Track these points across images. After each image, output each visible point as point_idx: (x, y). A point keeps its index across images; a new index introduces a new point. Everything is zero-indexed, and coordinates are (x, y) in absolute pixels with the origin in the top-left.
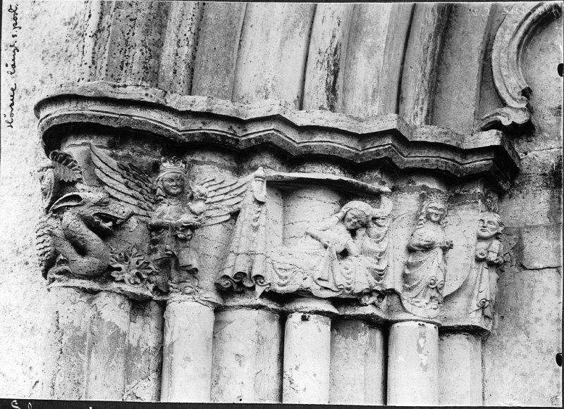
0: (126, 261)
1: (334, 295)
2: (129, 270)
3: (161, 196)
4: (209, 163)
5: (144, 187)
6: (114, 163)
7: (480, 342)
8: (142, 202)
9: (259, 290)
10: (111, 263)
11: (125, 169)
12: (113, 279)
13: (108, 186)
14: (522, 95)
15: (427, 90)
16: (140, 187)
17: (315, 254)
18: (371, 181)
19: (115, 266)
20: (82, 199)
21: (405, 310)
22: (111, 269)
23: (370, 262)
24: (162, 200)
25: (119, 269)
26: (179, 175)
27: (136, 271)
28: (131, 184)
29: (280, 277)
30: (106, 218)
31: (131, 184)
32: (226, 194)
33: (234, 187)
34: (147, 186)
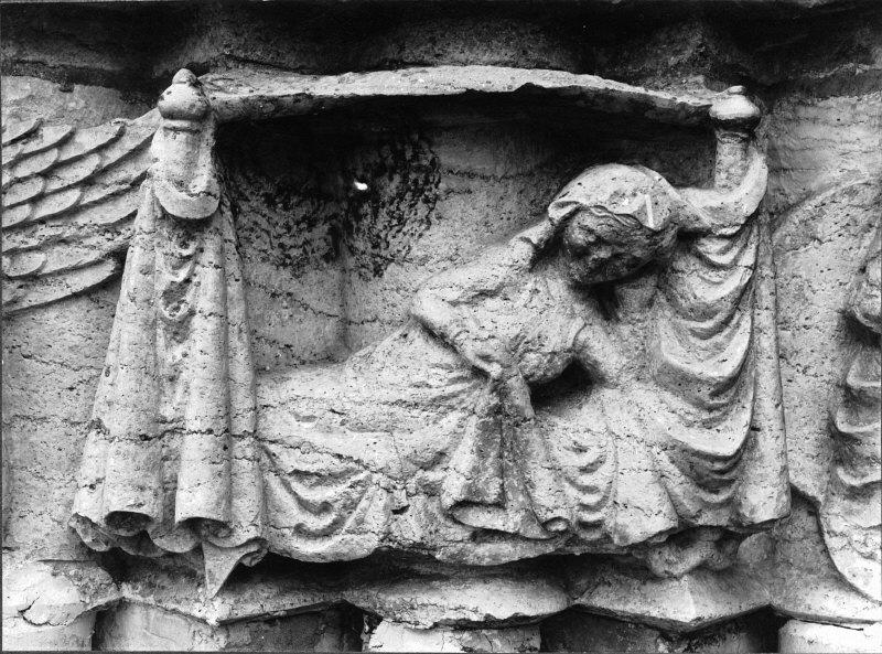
1: (531, 552)
9: (219, 566)
14: (140, 90)
15: (734, 389)
17: (440, 404)
18: (672, 75)
21: (840, 581)
23: (665, 416)
29: (304, 505)
33: (114, 155)
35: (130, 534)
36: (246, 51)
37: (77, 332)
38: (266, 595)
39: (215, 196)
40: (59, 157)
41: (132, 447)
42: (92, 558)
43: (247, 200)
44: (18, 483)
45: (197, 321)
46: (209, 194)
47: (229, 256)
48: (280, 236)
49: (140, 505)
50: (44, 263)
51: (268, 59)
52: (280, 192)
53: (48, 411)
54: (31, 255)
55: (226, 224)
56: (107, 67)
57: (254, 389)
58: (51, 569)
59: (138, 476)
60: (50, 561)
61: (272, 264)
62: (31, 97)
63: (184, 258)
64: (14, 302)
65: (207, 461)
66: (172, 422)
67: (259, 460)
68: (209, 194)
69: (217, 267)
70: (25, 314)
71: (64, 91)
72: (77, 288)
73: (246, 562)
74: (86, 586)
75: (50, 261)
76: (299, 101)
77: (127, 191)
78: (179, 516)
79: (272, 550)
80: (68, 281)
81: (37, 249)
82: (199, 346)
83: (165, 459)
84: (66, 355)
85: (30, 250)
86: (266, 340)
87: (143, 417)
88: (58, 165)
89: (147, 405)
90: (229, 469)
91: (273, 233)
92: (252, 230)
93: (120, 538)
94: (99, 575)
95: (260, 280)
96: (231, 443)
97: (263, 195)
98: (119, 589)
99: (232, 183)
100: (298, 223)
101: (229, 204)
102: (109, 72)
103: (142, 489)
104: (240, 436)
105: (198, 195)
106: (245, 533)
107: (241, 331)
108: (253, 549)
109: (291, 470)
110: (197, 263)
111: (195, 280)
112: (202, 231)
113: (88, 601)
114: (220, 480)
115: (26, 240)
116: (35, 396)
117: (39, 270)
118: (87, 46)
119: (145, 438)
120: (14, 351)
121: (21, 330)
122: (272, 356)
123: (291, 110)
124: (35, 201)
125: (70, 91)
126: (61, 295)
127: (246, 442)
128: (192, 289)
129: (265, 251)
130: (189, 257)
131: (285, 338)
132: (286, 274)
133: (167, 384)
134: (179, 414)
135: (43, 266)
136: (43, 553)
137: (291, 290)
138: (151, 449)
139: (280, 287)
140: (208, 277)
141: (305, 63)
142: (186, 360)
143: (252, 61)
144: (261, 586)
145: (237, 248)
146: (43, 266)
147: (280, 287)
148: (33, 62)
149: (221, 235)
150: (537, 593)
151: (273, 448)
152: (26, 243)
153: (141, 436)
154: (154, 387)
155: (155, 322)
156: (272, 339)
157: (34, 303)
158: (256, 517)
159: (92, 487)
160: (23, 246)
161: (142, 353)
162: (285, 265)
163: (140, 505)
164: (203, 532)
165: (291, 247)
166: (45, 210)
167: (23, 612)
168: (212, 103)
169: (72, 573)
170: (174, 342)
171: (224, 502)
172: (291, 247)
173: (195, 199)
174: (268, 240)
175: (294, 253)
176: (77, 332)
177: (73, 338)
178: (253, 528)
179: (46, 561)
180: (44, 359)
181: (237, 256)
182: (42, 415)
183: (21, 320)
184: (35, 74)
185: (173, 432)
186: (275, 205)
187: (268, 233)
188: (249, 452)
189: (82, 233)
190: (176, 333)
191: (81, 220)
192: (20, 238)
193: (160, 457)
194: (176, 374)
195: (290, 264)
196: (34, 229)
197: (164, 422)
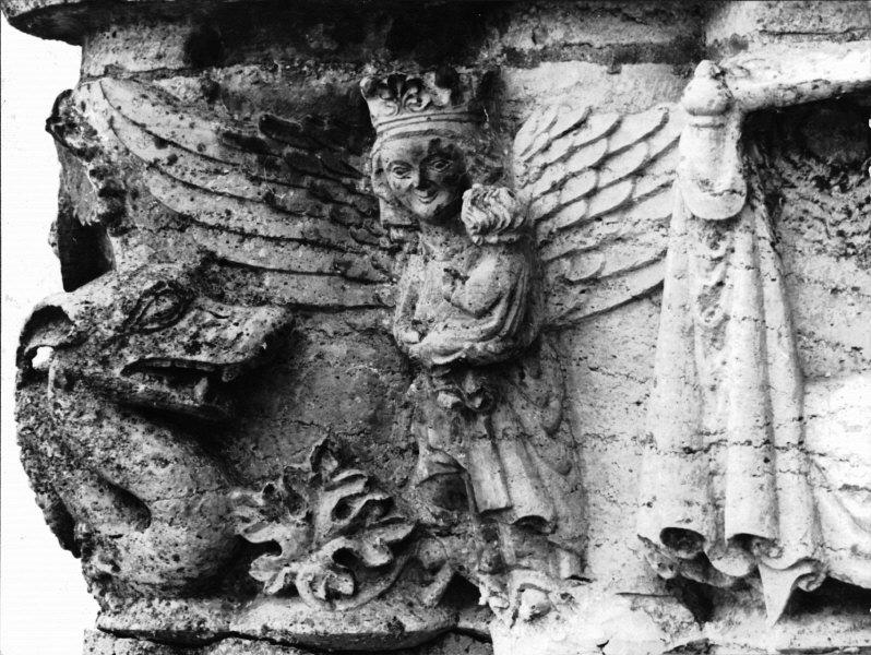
0: (294, 509)
2: (309, 544)
5: (341, 195)
6: (205, 132)
7: (756, 613)
8: (347, 257)
9: (777, 589)
10: (240, 528)
11: (250, 145)
13: (204, 226)
16: (327, 199)
19: (257, 538)
20: (47, 372)
25: (273, 547)
26: (425, 142)
27: (339, 543)
28: (288, 197)
30: (182, 374)
32: (639, 173)
35: (690, 556)
36: (782, 23)
37: (641, 339)
38: (836, 628)
39: (740, 193)
40: (608, 147)
41: (676, 461)
42: (672, 593)
43: (793, 186)
44: (592, 508)
45: (732, 326)
46: (734, 191)
47: (764, 254)
48: (837, 223)
49: (688, 521)
50: (603, 264)
51: (809, 28)
52: (835, 172)
53: (616, 428)
54: (590, 255)
55: (758, 220)
56: (656, 40)
57: (801, 396)
58: (630, 603)
59: (685, 492)
60: (628, 594)
61: (831, 256)
62: (578, 83)
63: (716, 260)
64: (577, 309)
65: (747, 474)
66: (715, 433)
67: (806, 474)
68: (734, 191)
69: (748, 268)
70: (590, 322)
71: (612, 74)
72: (637, 291)
73: (803, 585)
74: (667, 624)
75: (609, 263)
76: (816, 87)
78: (729, 533)
79: (832, 575)
80: (628, 284)
81: (596, 249)
82: (735, 352)
83: (713, 474)
84: (631, 366)
85: (588, 250)
86: (828, 343)
87: (685, 428)
88: (608, 157)
89: (689, 416)
90: (773, 482)
91: (829, 219)
92: (801, 219)
93: (682, 561)
94: (681, 612)
95: (814, 276)
96: (774, 455)
97: (813, 179)
98: (701, 629)
99: (773, 171)
100: (860, 206)
101: (762, 197)
102: (659, 46)
103: (689, 504)
104: (783, 448)
105: (721, 195)
106: (794, 552)
107: (780, 335)
108: (807, 569)
109: (840, 485)
110: (728, 264)
111: (728, 282)
112: (732, 230)
113: (668, 639)
114: (762, 494)
115: (584, 239)
116: (603, 412)
117: (598, 273)
118: (634, 19)
119: (689, 451)
120: (581, 363)
121: (586, 340)
122: (836, 361)
123: (812, 96)
124: (590, 195)
125: (618, 72)
126: (622, 300)
127: (789, 455)
128: (724, 291)
129: (820, 242)
130: (720, 259)
131: (850, 341)
132: (849, 265)
133: (709, 394)
134: (721, 426)
135: (602, 268)
136: (620, 585)
137: (856, 285)
138: (697, 462)
139: (843, 281)
140: (739, 278)
141: (854, 24)
142: (726, 367)
143: (789, 33)
144: (832, 619)
145: (773, 245)
146: (602, 268)
147: (843, 281)
148: (581, 44)
149: (753, 233)
150: (110, 252)
151: (821, 461)
152: (585, 243)
153: (685, 449)
154: (695, 397)
155: (692, 328)
156: (834, 342)
157: (596, 310)
158: (806, 535)
159: (649, 505)
160: (582, 247)
161: (681, 363)
162: (846, 255)
163: (688, 521)
164: (756, 551)
165: (854, 234)
166: (601, 204)
167: (602, 646)
168: (736, 94)
169: (651, 609)
170: (712, 349)
171: (768, 518)
172: (854, 234)
173: (718, 199)
174: (823, 229)
175: (857, 240)
176: (641, 339)
177: (637, 347)
178: (804, 547)
179: (623, 594)
180: (609, 371)
181: (773, 254)
182: (611, 433)
183: (585, 328)
184: (582, 58)
185: (718, 444)
186: (829, 187)
187: (823, 220)
188: (794, 466)
189: (638, 229)
190: (714, 340)
191: (635, 214)
192: (579, 237)
193: (707, 472)
194: (716, 383)
195: (854, 254)
196: (591, 227)
197: (708, 434)
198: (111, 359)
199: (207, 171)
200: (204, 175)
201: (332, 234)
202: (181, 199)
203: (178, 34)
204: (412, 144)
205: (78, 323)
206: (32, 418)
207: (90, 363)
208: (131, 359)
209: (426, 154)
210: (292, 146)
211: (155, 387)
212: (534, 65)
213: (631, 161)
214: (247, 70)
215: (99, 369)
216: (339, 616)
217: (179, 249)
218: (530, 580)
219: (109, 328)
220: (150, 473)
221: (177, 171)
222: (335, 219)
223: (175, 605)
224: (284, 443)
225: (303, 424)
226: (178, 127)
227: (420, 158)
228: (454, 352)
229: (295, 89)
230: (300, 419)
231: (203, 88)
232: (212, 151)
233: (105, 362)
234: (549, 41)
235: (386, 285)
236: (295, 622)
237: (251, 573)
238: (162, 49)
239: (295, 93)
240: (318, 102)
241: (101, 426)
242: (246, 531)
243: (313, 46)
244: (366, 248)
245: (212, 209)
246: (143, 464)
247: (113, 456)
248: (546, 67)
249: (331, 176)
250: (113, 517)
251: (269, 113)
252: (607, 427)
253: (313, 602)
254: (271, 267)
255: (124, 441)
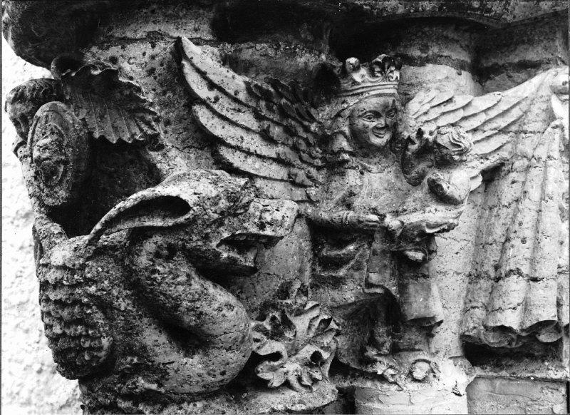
2: (294, 351)
3: (346, 152)
4: (435, 60)
6: (237, 83)
10: (255, 346)
12: (264, 386)
19: (262, 352)
22: (256, 359)
24: (347, 161)
25: (276, 356)
26: (390, 100)
31: (276, 131)
33: (493, 114)
34: (307, 129)
62: (447, 78)
77: (496, 134)
116: (441, 259)
179: (450, 358)
182: (445, 270)
198: (210, 235)
199: (234, 109)
200: (233, 112)
201: (291, 156)
202: (217, 126)
203: (206, 17)
204: (384, 101)
205: (195, 208)
206: (106, 282)
207: (195, 238)
208: (226, 235)
209: (390, 108)
210: (287, 99)
211: (232, 254)
212: (422, 64)
213: (475, 123)
214: (258, 46)
215: (199, 243)
216: (315, 394)
217: (199, 161)
218: (422, 357)
219: (215, 212)
220: (224, 315)
221: (218, 108)
222: (295, 148)
223: (199, 405)
224: (258, 288)
225: (269, 274)
226: (226, 77)
227: (386, 110)
228: (441, 225)
229: (288, 62)
230: (268, 271)
231: (221, 55)
232: (242, 96)
233: (206, 238)
234: (430, 53)
235: (312, 188)
236: (295, 404)
237: (260, 375)
238: (197, 26)
239: (288, 65)
240: (298, 72)
241: (191, 285)
242: (259, 348)
243: (302, 36)
244: (304, 166)
245: (233, 136)
246: (219, 309)
247: (198, 306)
248: (430, 66)
249: (299, 119)
250: (168, 349)
251: (270, 76)
252: (442, 267)
253: (301, 388)
254: (261, 175)
255: (206, 295)
